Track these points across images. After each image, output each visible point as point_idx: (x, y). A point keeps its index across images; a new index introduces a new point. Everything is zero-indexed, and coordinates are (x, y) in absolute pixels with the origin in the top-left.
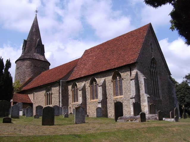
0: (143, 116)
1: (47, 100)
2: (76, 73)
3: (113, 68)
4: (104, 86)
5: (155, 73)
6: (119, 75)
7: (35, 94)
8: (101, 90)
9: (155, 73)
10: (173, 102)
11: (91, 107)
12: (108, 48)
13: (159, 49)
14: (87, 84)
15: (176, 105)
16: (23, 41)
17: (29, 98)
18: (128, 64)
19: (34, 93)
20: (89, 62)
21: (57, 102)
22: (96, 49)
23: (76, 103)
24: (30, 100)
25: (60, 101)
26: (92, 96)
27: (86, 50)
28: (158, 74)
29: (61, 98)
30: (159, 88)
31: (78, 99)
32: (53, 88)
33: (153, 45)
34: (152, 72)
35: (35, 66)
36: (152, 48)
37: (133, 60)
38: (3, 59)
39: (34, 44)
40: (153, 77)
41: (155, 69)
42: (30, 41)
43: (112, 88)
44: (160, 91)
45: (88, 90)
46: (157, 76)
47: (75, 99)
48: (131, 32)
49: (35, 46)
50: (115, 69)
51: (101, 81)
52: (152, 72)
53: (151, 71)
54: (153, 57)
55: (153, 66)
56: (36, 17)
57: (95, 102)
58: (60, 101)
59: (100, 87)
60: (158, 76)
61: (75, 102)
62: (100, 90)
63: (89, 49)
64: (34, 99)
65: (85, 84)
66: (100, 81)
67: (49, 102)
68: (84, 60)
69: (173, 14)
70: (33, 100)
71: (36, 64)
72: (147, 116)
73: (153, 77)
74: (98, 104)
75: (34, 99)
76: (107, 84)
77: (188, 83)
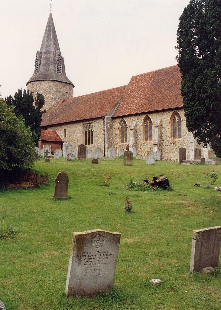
0: (203, 160)
1: (86, 138)
2: (123, 108)
3: (172, 107)
4: (160, 127)
6: (178, 116)
7: (66, 130)
8: (158, 131)
11: (143, 149)
14: (139, 122)
17: (58, 135)
19: (65, 129)
20: (140, 95)
21: (101, 142)
22: (147, 77)
23: (124, 143)
24: (60, 138)
25: (104, 141)
26: (145, 137)
27: (133, 77)
29: (106, 138)
31: (128, 139)
32: (93, 124)
34: (87, 133)
35: (57, 91)
39: (51, 63)
42: (45, 53)
43: (170, 130)
45: (141, 129)
47: (123, 138)
49: (54, 61)
52: (87, 133)
53: (56, 54)
56: (51, 14)
58: (104, 141)
61: (123, 142)
62: (156, 133)
63: (138, 76)
64: (65, 137)
65: (136, 123)
66: (155, 119)
68: (132, 92)
69: (41, 120)
70: (64, 137)
71: (57, 87)
72: (206, 160)
75: (65, 137)
76: (164, 125)
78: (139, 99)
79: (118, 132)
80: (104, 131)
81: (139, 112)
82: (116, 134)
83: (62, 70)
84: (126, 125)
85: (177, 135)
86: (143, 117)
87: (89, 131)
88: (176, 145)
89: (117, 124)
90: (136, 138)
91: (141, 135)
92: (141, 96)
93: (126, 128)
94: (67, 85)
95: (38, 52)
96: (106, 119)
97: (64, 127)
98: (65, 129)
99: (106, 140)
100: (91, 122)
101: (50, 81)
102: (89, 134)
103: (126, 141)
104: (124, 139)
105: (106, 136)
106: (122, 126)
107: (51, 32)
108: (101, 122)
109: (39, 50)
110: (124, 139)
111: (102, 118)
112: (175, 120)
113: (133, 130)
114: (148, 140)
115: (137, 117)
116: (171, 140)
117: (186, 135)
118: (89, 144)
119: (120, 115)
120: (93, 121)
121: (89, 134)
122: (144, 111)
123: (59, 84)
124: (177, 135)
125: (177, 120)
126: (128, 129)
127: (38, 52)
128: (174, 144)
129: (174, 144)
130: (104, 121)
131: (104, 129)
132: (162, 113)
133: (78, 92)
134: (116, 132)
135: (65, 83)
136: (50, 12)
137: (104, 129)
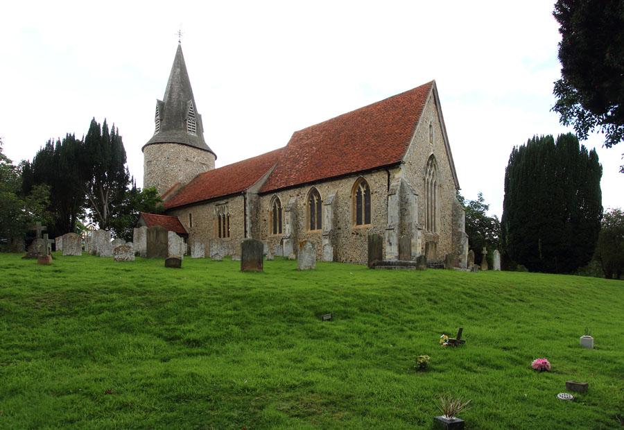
5: (431, 184)
7: (192, 216)
9: (431, 184)
10: (459, 240)
12: (343, 131)
13: (444, 138)
15: (463, 246)
16: (156, 102)
18: (385, 164)
19: (190, 215)
20: (304, 156)
25: (246, 232)
27: (296, 133)
28: (437, 187)
30: (437, 213)
31: (283, 228)
33: (434, 128)
34: (222, 218)
35: (187, 160)
36: (431, 136)
37: (395, 157)
38: (74, 135)
39: (177, 115)
40: (428, 194)
41: (433, 176)
43: (351, 210)
44: (438, 220)
46: (435, 190)
48: (392, 97)
50: (357, 173)
51: (330, 196)
52: (222, 218)
54: (432, 153)
55: (430, 171)
56: (180, 49)
57: (316, 234)
58: (246, 232)
59: (326, 207)
60: (436, 191)
64: (191, 226)
67: (224, 232)
73: (428, 194)
74: (322, 238)
75: (191, 226)
77: (606, 115)
78: (302, 163)
79: (268, 217)
80: (245, 215)
81: (301, 181)
82: (265, 220)
83: (195, 125)
84: (280, 205)
85: (363, 219)
86: (307, 190)
87: (224, 215)
88: (361, 236)
89: (267, 204)
90: (296, 226)
91: (304, 222)
92: (305, 159)
93: (280, 210)
94: (204, 152)
95: (159, 101)
96: (247, 196)
97: (190, 211)
98: (190, 215)
99: (248, 229)
100: (226, 201)
101: (175, 145)
102: (224, 222)
103: (280, 232)
104: (278, 228)
105: (248, 223)
106: (275, 207)
107: (180, 49)
108: (240, 199)
109: (162, 100)
110: (278, 228)
111: (241, 193)
112: (359, 193)
113: (289, 212)
114: (361, 224)
115: (297, 191)
116: (353, 227)
117: (379, 217)
118: (224, 236)
119: (271, 188)
120: (229, 200)
121: (224, 222)
122: (309, 179)
123: (190, 150)
124: (363, 219)
125: (363, 193)
126: (283, 211)
127: (159, 101)
128: (357, 234)
129: (357, 234)
130: (245, 199)
131: (245, 212)
132: (337, 182)
133: (219, 164)
134: (265, 218)
135: (201, 149)
136: (178, 43)
137: (245, 212)
